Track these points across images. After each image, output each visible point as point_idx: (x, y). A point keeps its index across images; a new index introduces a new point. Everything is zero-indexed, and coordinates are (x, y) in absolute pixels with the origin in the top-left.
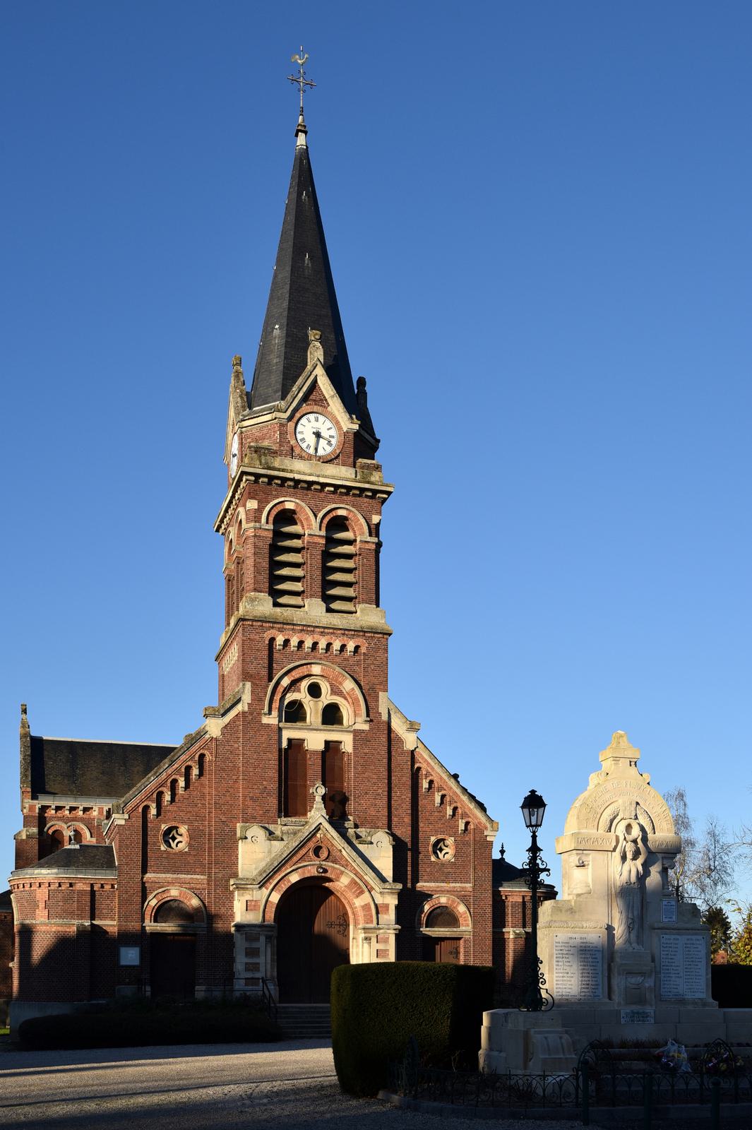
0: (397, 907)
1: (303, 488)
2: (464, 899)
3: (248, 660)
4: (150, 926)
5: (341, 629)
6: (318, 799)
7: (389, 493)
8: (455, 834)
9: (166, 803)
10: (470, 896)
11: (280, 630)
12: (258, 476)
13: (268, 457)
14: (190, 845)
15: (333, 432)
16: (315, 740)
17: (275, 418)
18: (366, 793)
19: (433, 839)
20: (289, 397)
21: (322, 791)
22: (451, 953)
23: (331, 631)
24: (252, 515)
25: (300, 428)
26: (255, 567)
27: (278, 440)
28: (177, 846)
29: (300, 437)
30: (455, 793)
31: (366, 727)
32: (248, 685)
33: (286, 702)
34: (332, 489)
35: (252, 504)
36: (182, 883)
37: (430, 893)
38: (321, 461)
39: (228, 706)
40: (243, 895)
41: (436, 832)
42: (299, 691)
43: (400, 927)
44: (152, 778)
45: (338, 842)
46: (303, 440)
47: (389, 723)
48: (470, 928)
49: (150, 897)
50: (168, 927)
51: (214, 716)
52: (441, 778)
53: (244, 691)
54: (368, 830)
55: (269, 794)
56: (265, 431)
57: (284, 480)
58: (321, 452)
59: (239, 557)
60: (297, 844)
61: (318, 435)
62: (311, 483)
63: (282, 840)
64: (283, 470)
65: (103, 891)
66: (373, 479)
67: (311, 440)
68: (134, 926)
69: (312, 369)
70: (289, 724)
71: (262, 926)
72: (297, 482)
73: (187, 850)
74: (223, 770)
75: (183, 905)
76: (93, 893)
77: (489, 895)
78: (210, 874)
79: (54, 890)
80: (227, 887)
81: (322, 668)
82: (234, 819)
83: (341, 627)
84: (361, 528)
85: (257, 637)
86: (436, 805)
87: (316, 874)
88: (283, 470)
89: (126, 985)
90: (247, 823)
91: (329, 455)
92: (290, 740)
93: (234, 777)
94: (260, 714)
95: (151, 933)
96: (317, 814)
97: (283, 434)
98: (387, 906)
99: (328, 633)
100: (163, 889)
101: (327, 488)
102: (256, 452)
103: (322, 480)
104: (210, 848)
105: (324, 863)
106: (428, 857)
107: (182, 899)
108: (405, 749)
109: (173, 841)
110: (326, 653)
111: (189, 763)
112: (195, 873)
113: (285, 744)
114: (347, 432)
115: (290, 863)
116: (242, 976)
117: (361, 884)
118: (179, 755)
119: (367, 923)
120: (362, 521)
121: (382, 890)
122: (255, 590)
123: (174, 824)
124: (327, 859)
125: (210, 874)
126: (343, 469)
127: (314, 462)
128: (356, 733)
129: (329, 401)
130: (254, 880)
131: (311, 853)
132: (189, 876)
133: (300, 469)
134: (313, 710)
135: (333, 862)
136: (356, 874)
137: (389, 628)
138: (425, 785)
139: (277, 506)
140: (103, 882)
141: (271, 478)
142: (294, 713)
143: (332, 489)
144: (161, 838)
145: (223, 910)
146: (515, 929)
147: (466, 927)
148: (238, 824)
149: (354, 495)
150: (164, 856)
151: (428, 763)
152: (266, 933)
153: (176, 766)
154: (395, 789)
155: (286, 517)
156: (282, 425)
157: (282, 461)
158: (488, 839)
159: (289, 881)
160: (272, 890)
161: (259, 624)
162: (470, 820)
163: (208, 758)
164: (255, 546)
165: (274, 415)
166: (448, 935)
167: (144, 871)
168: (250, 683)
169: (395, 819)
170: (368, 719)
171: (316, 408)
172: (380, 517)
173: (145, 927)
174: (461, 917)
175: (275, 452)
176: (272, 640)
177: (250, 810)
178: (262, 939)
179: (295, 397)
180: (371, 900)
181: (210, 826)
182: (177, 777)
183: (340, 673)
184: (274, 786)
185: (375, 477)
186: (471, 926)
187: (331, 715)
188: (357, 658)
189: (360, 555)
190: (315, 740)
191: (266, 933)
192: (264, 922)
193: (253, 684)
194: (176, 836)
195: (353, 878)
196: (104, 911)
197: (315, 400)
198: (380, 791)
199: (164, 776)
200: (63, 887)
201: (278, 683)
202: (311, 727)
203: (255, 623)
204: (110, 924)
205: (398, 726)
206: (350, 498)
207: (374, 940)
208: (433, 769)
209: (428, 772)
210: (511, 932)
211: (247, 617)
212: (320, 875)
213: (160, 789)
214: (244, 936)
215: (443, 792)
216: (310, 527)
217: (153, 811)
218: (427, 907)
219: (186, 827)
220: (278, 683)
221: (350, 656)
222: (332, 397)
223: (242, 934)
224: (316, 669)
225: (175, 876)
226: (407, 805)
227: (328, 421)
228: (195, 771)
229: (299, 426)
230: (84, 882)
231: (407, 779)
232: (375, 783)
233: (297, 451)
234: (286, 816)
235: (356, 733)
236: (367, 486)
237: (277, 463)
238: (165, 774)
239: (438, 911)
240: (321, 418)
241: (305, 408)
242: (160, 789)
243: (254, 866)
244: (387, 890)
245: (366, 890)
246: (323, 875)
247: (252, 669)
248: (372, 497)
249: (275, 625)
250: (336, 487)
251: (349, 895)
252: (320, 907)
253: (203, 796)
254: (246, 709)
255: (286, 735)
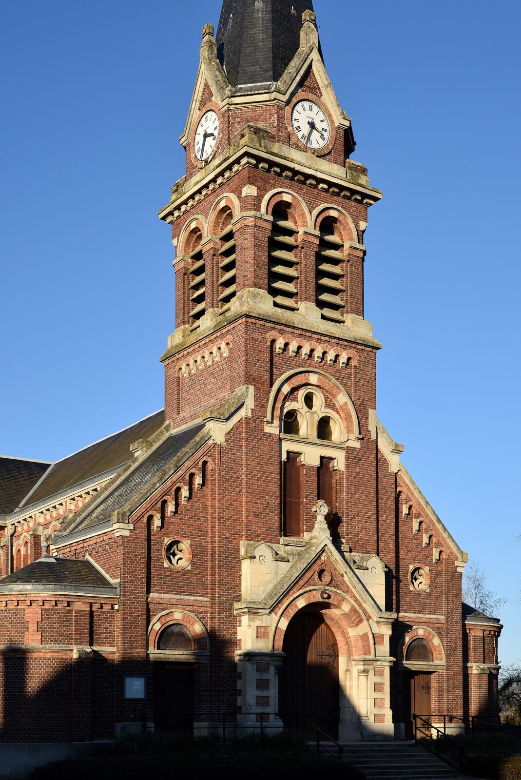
0: (391, 638)
1: (299, 181)
2: (438, 630)
3: (251, 361)
4: (154, 653)
5: (336, 338)
6: (320, 518)
7: (376, 199)
8: (429, 564)
9: (169, 514)
10: (442, 628)
11: (281, 332)
12: (259, 159)
13: (267, 141)
14: (192, 563)
15: (325, 125)
16: (311, 456)
17: (275, 99)
18: (358, 515)
19: (411, 568)
20: (285, 76)
21: (325, 510)
22: (423, 688)
23: (327, 339)
24: (250, 202)
25: (296, 115)
26: (255, 259)
27: (275, 124)
28: (177, 564)
29: (295, 124)
30: (431, 521)
31: (357, 445)
32: (252, 388)
33: (285, 411)
34: (326, 187)
35: (249, 190)
36: (185, 605)
37: (409, 623)
38: (316, 154)
39: (232, 410)
40: (253, 621)
41: (414, 560)
42: (297, 400)
43: (394, 659)
44: (158, 485)
45: (342, 567)
46: (298, 128)
47: (377, 442)
48: (443, 662)
49: (154, 620)
50: (178, 654)
51: (218, 419)
52: (420, 504)
53: (247, 396)
54: (361, 555)
55: (271, 511)
56: (259, 112)
57: (284, 168)
58: (314, 145)
59: (215, 248)
60: (305, 566)
61: (312, 125)
62: (308, 176)
63: (288, 561)
64: (285, 158)
65: (101, 612)
66: (360, 182)
67: (306, 129)
68: (138, 652)
69: (309, 52)
70: (288, 436)
71: (272, 655)
72: (296, 173)
73: (189, 568)
74: (227, 480)
75: (185, 630)
76: (91, 613)
77: (459, 627)
78: (213, 595)
79: (48, 609)
80: (230, 611)
81: (318, 378)
82: (237, 535)
83: (337, 336)
84: (350, 233)
85: (259, 337)
86: (414, 532)
87: (320, 600)
88: (285, 158)
89: (131, 721)
90: (250, 540)
91: (322, 149)
92: (288, 452)
93: (237, 490)
94: (262, 422)
95: (154, 661)
96: (320, 534)
97: (280, 118)
98: (382, 636)
99: (324, 341)
100: (167, 611)
101: (321, 185)
102: (255, 133)
103: (320, 175)
104: (213, 567)
105: (327, 588)
106: (407, 586)
107: (185, 624)
108: (390, 471)
109: (174, 557)
110: (321, 362)
111: (193, 471)
112: (197, 594)
113: (284, 457)
114: (339, 127)
115: (297, 586)
116: (252, 711)
117: (361, 612)
118: (184, 460)
119: (366, 654)
120: (352, 226)
121: (379, 619)
122: (255, 285)
123: (177, 538)
124: (329, 584)
125: (213, 595)
126: (336, 166)
127: (309, 154)
128: (349, 451)
129: (323, 90)
130: (266, 604)
131: (316, 577)
132: (192, 598)
133: (299, 160)
134: (307, 426)
135: (335, 587)
136: (356, 600)
137: (377, 342)
138: (405, 510)
139: (276, 196)
140: (102, 602)
141: (272, 164)
142: (290, 423)
143: (326, 187)
144: (164, 553)
145: (227, 636)
146: (477, 664)
147: (439, 661)
148: (241, 542)
149: (345, 197)
150: (168, 573)
151: (409, 488)
152: (275, 663)
153: (180, 473)
154: (381, 513)
155: (281, 210)
156: (280, 108)
157: (280, 148)
158: (459, 570)
159: (296, 606)
160: (281, 615)
161: (262, 322)
162: (443, 549)
163: (210, 466)
164: (255, 238)
165: (273, 96)
166: (425, 668)
167: (148, 591)
168: (253, 387)
169: (381, 544)
170: (361, 436)
171: (311, 96)
172: (366, 224)
173: (149, 654)
174: (435, 650)
175: (273, 137)
176: (273, 341)
177: (253, 527)
178: (272, 669)
179: (294, 79)
180: (369, 629)
181: (213, 542)
182: (181, 485)
183: (335, 385)
184: (275, 502)
185: (363, 180)
186: (444, 659)
187: (323, 428)
188: (348, 371)
189: (348, 261)
190: (311, 456)
191: (275, 663)
192: (274, 651)
193: (256, 388)
194: (176, 551)
195: (353, 606)
196: (102, 636)
197: (309, 87)
198: (370, 514)
199: (169, 483)
200: (60, 607)
201: (279, 390)
202: (309, 441)
203: (257, 322)
204: (111, 651)
205: (385, 447)
206: (340, 199)
207: (371, 673)
208: (412, 494)
209: (408, 497)
210: (475, 668)
211: (252, 314)
212: (324, 600)
213: (165, 498)
214: (255, 666)
215: (421, 519)
216: (305, 224)
217: (157, 522)
218: (407, 639)
219: (189, 542)
220: (279, 390)
221: (342, 368)
222: (326, 86)
223: (253, 664)
224: (313, 379)
225: (178, 597)
226: (391, 531)
227: (320, 113)
228: (198, 480)
229: (295, 112)
230: (83, 601)
231: (391, 504)
232: (365, 505)
233: (293, 140)
234: (285, 535)
235: (349, 451)
236: (359, 189)
237: (276, 148)
238: (169, 480)
239: (415, 643)
240: (315, 108)
241: (301, 94)
242: (165, 498)
243: (261, 589)
244: (383, 620)
245: (364, 618)
246: (327, 600)
247: (255, 371)
248: (360, 202)
249: (277, 326)
250: (331, 184)
251: (344, 623)
252: (311, 638)
253: (205, 508)
254: (250, 415)
255: (286, 446)
